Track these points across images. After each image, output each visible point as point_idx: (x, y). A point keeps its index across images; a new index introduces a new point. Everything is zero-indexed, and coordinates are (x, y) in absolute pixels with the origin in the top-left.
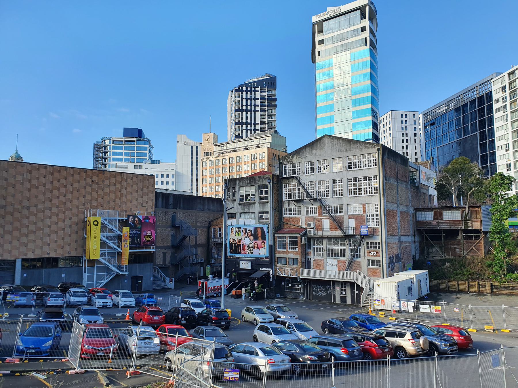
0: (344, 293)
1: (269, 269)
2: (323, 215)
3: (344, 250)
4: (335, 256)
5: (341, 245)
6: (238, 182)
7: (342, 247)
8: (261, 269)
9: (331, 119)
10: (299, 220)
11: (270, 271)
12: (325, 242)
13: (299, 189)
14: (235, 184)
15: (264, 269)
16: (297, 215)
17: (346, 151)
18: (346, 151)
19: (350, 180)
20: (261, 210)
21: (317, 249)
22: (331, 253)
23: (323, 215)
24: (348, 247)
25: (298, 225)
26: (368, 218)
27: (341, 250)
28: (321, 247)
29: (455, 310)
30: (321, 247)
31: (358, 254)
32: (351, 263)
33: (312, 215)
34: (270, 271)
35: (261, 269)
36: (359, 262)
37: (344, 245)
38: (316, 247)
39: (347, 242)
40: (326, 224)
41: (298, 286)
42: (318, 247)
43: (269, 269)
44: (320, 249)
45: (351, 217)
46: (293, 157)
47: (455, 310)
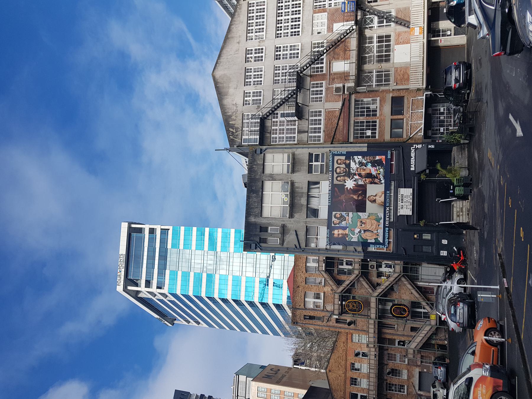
0: (449, 33)
1: (413, 151)
2: (324, 72)
3: (379, 37)
4: (389, 51)
5: (371, 42)
6: (252, 219)
7: (375, 40)
8: (413, 169)
9: (224, 280)
10: (329, 113)
11: (416, 149)
12: (367, 67)
13: (283, 115)
14: (255, 224)
15: (413, 161)
16: (322, 118)
17: (239, 43)
18: (239, 43)
19: (278, 36)
20: (306, 168)
21: (377, 81)
22: (385, 57)
23: (324, 72)
24: (375, 30)
25: (338, 114)
26: (333, 5)
27: (379, 42)
28: (375, 74)
29: (454, 248)
30: (375, 74)
31: (385, 24)
32: (399, 22)
33: (324, 92)
34: (416, 149)
35: (413, 169)
36: (398, 11)
37: (371, 38)
38: (374, 84)
39: (368, 33)
40: (340, 66)
41: (443, 113)
42: (374, 79)
43: (413, 151)
44: (378, 76)
45: (330, 29)
46: (233, 126)
47: (454, 248)
